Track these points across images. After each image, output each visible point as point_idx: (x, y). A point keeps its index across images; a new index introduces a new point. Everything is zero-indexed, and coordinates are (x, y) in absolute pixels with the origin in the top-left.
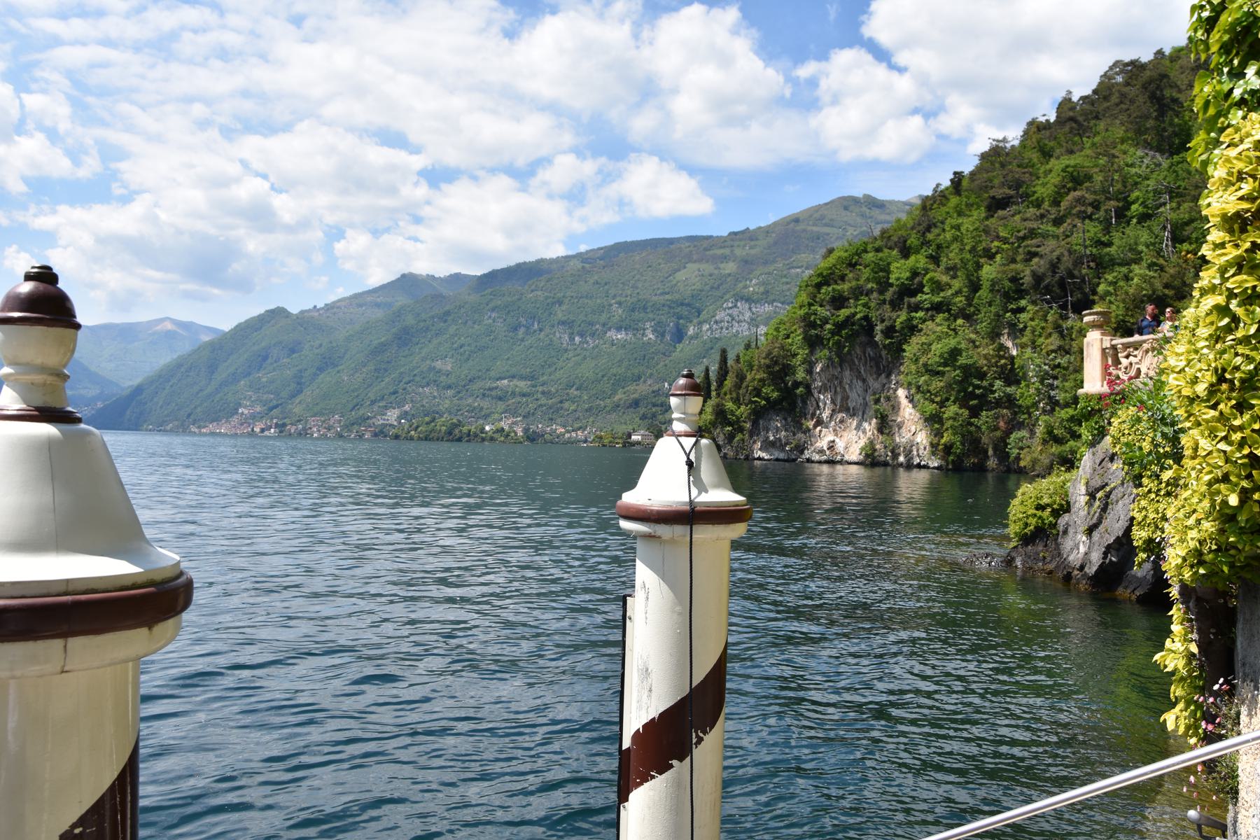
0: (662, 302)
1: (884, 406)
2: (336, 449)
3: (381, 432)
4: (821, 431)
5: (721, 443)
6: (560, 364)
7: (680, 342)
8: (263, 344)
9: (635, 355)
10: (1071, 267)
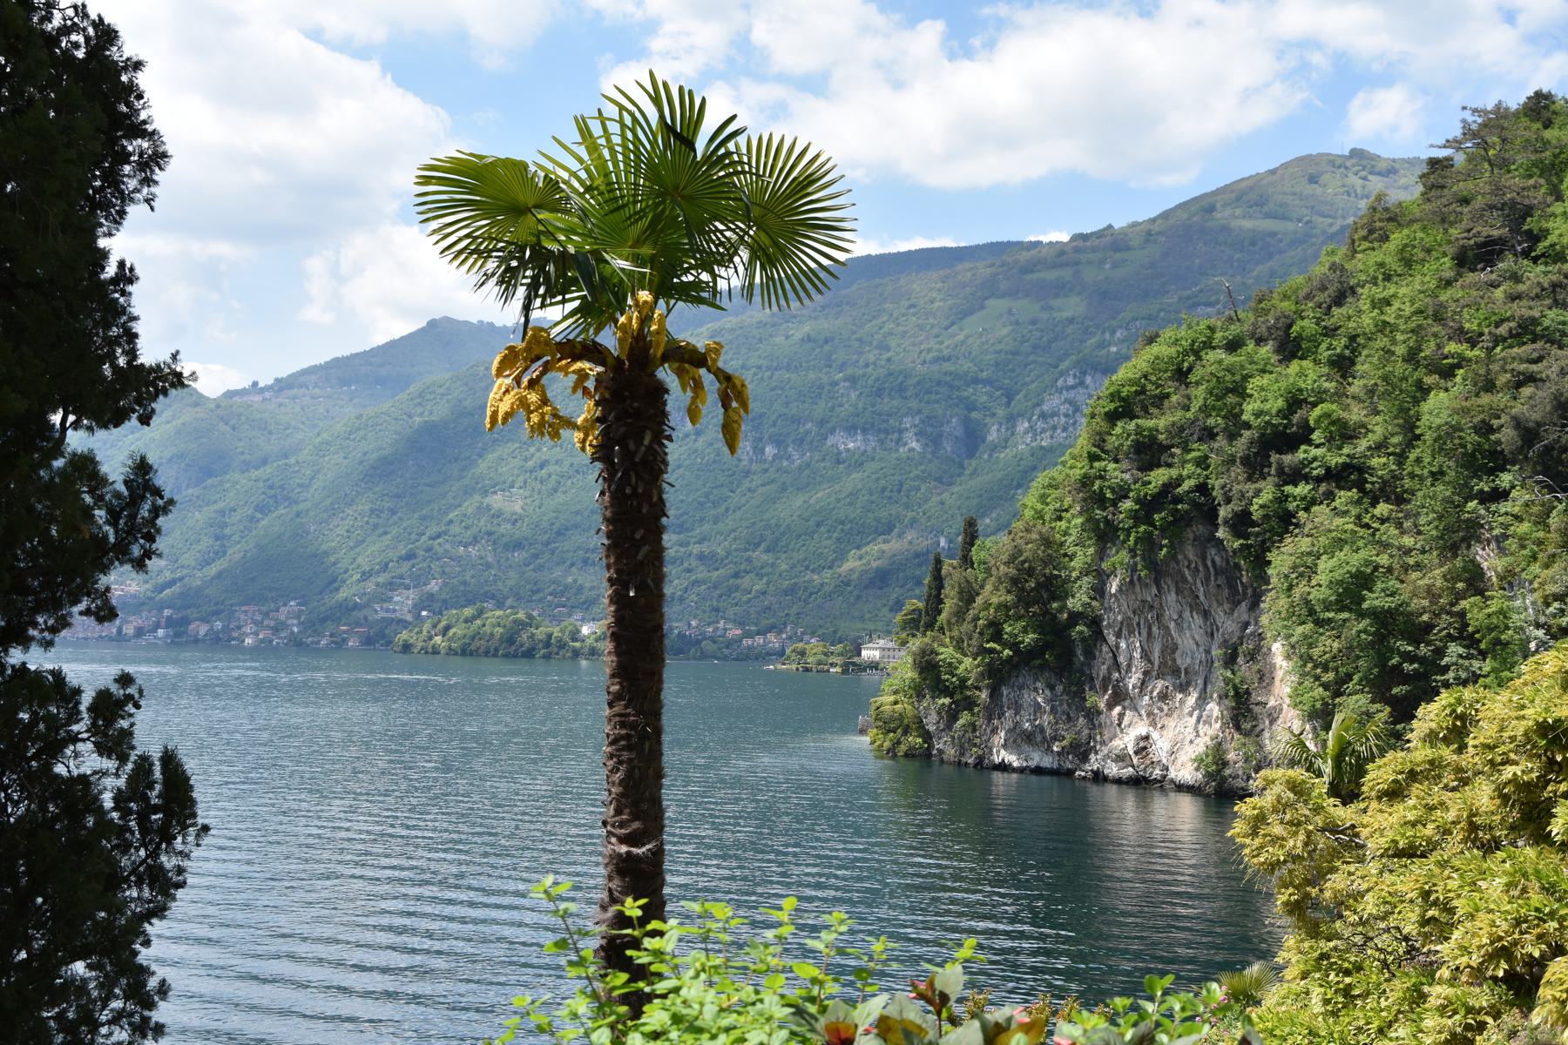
1: (1244, 669)
2: (495, 581)
3: (381, 635)
4: (1121, 716)
5: (931, 728)
7: (971, 455)
9: (882, 482)
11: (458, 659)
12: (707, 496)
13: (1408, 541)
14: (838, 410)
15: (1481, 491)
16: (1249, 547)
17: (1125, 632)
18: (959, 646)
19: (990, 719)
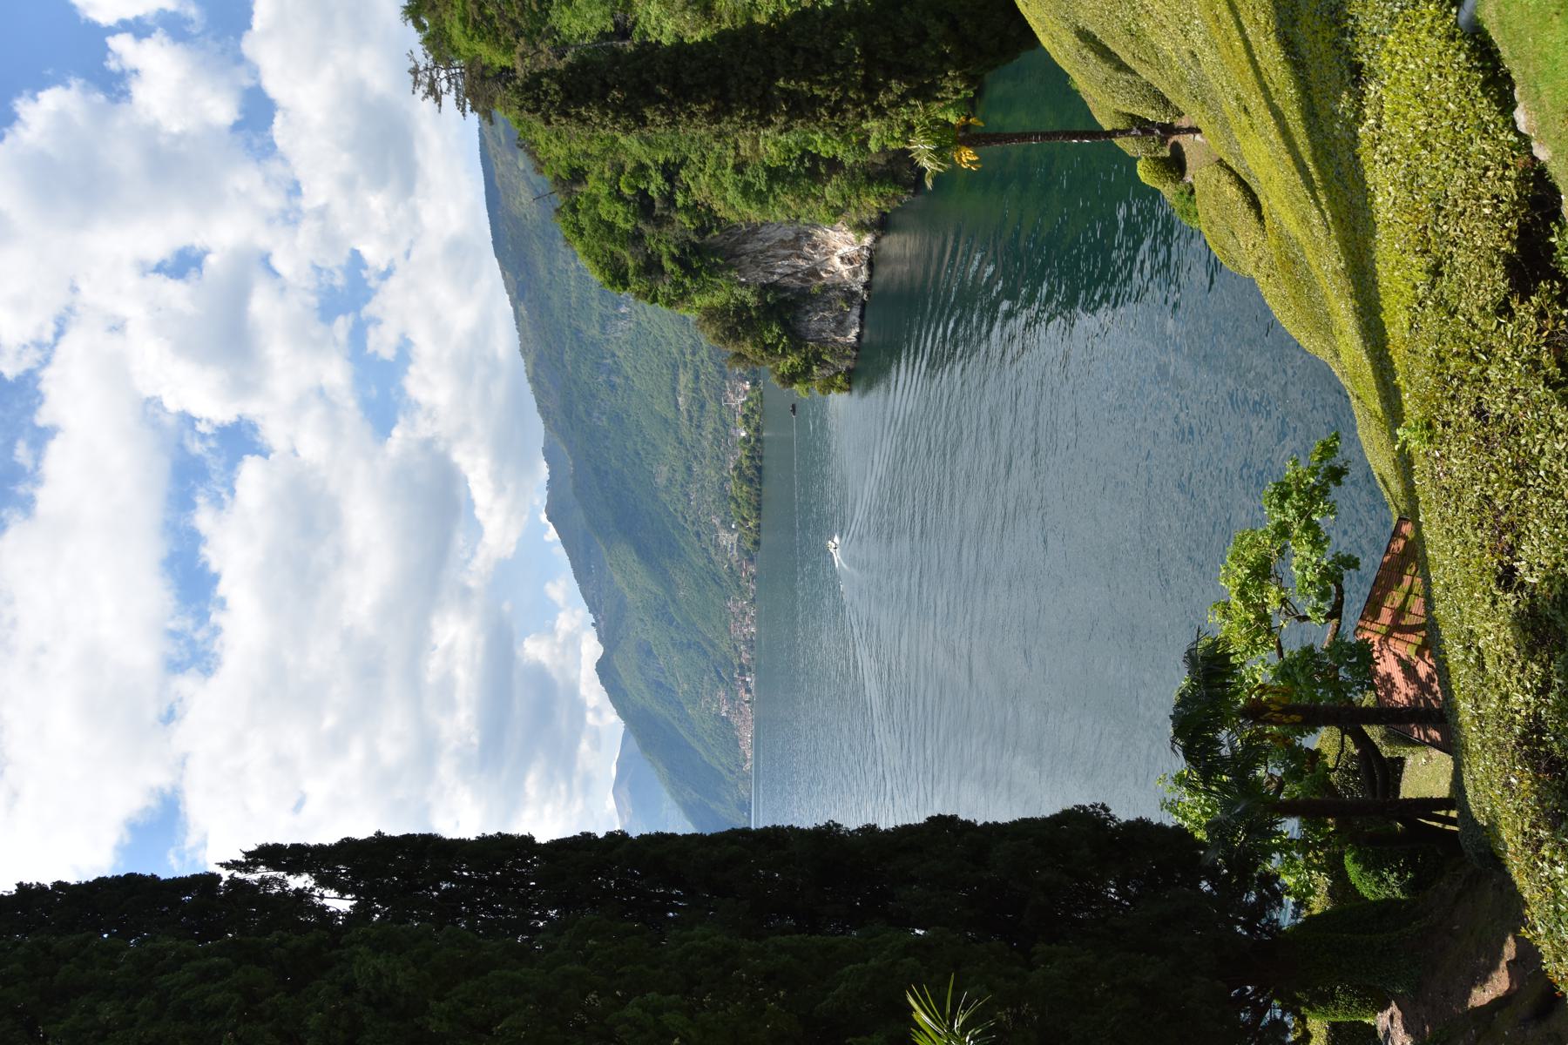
5: (832, 372)
6: (656, 331)
8: (642, 687)
11: (763, 513)
12: (654, 350)
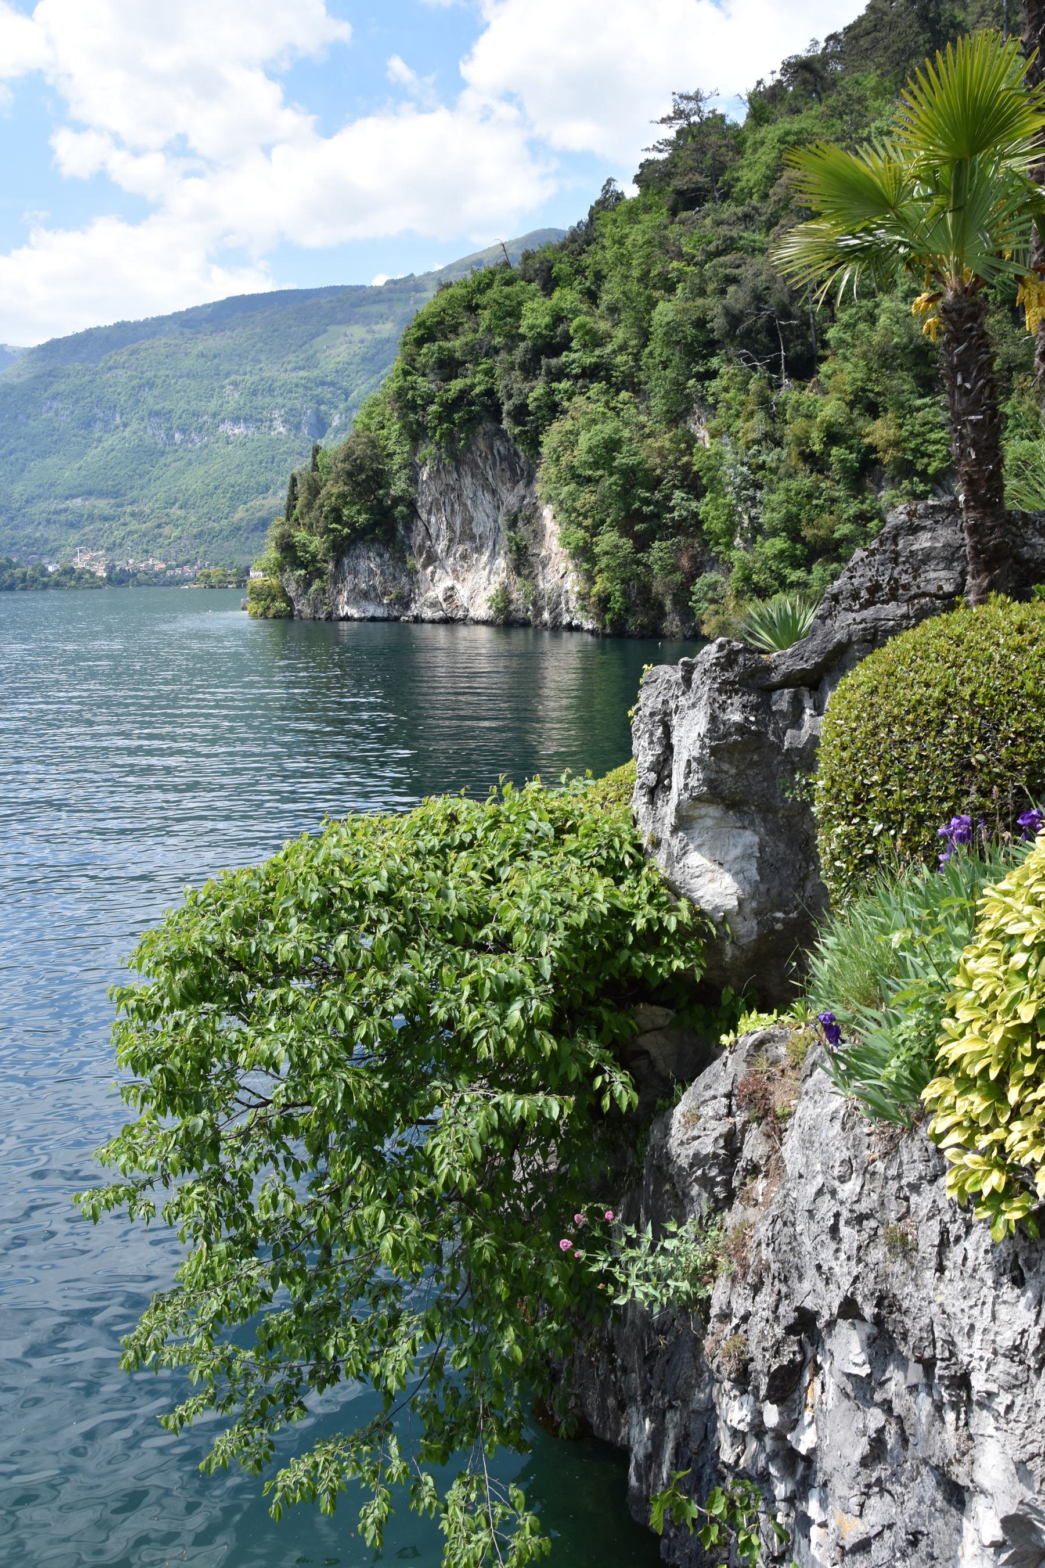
0: (295, 381)
1: (522, 529)
4: (433, 573)
5: (292, 594)
6: (155, 472)
9: (260, 457)
10: (787, 301)
13: (643, 418)
14: (226, 406)
15: (698, 372)
16: (526, 432)
17: (434, 510)
18: (310, 528)
19: (335, 583)
